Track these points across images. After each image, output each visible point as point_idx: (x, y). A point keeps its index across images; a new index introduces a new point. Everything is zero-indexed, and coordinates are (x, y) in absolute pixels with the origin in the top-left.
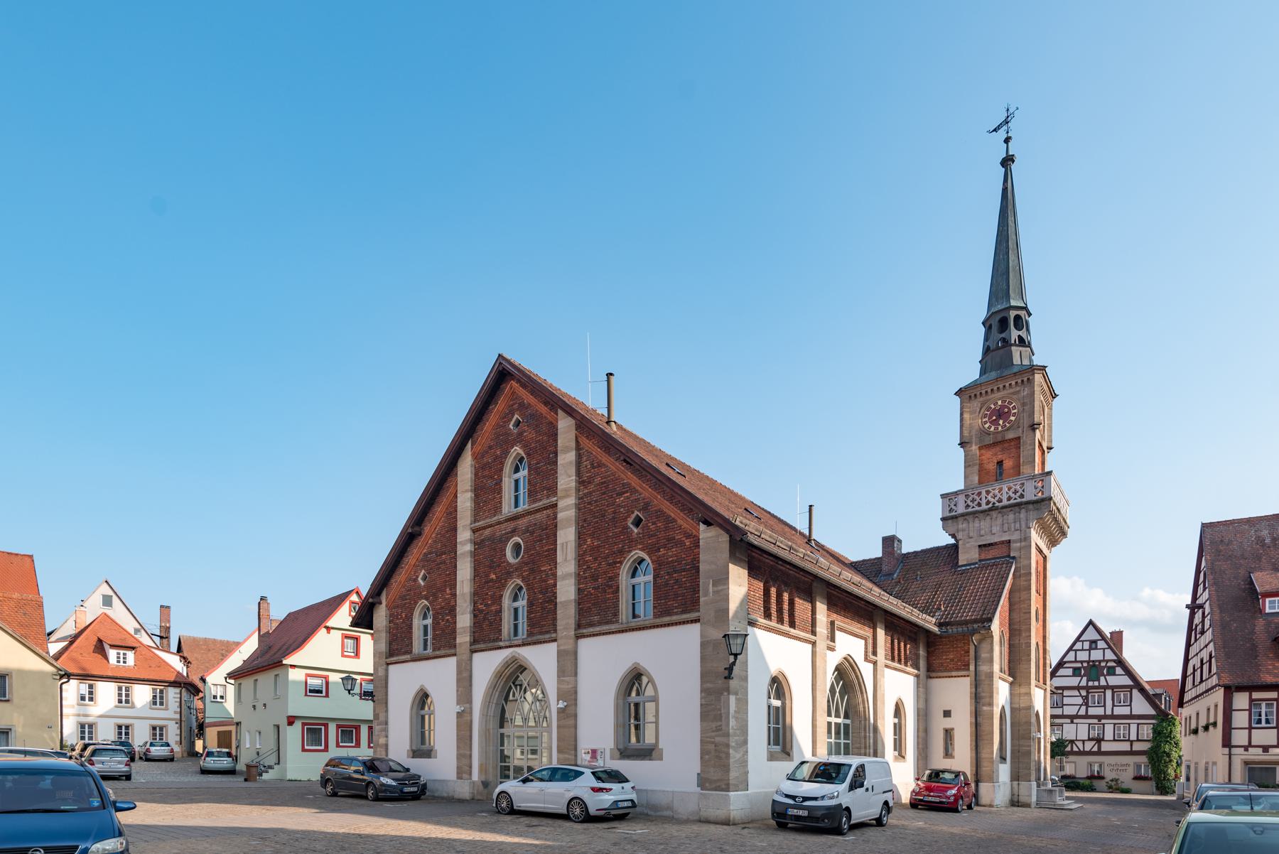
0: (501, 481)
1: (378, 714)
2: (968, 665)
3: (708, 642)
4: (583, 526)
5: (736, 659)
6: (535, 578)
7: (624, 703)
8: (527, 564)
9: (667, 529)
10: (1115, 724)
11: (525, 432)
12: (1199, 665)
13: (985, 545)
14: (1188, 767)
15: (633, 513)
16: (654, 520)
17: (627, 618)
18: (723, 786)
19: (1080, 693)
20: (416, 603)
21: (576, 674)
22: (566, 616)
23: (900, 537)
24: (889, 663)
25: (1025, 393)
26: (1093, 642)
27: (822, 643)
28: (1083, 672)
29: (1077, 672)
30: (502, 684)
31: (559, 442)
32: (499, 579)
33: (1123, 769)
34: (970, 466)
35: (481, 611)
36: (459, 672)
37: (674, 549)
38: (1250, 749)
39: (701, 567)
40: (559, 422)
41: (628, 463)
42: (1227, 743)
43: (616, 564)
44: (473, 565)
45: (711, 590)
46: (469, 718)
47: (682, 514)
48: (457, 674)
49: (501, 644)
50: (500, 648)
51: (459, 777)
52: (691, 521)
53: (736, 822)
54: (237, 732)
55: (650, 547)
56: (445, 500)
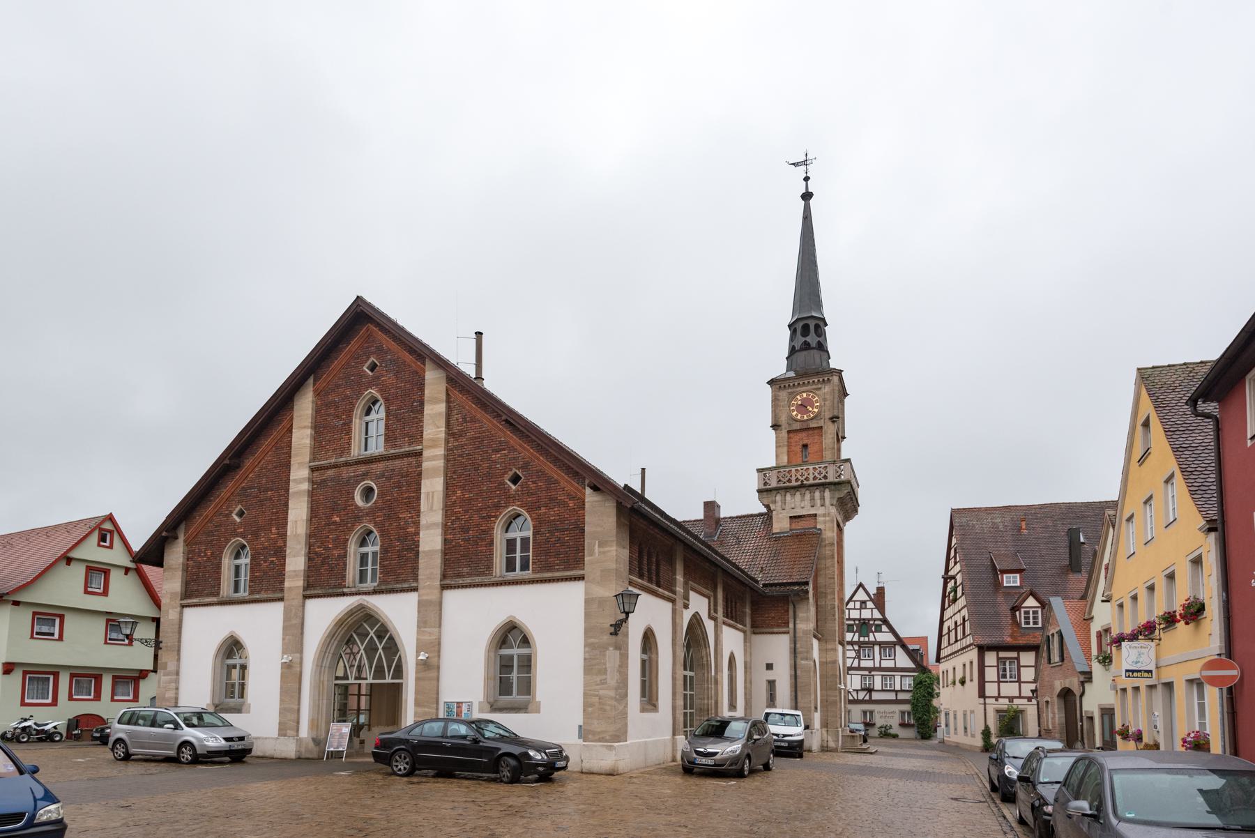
0: (351, 422)
2: (788, 623)
3: (593, 599)
7: (495, 656)
8: (381, 509)
9: (548, 489)
12: (953, 627)
13: (795, 517)
14: (947, 714)
17: (501, 571)
18: (608, 738)
20: (227, 541)
21: (440, 626)
25: (826, 390)
26: (863, 603)
27: (680, 603)
28: (855, 628)
29: (851, 628)
30: (342, 632)
32: (344, 523)
33: (889, 716)
34: (780, 446)
36: (287, 619)
37: (555, 509)
38: (1000, 699)
42: (982, 694)
43: (489, 518)
44: (310, 505)
48: (284, 621)
49: (345, 590)
50: (344, 594)
55: (530, 504)
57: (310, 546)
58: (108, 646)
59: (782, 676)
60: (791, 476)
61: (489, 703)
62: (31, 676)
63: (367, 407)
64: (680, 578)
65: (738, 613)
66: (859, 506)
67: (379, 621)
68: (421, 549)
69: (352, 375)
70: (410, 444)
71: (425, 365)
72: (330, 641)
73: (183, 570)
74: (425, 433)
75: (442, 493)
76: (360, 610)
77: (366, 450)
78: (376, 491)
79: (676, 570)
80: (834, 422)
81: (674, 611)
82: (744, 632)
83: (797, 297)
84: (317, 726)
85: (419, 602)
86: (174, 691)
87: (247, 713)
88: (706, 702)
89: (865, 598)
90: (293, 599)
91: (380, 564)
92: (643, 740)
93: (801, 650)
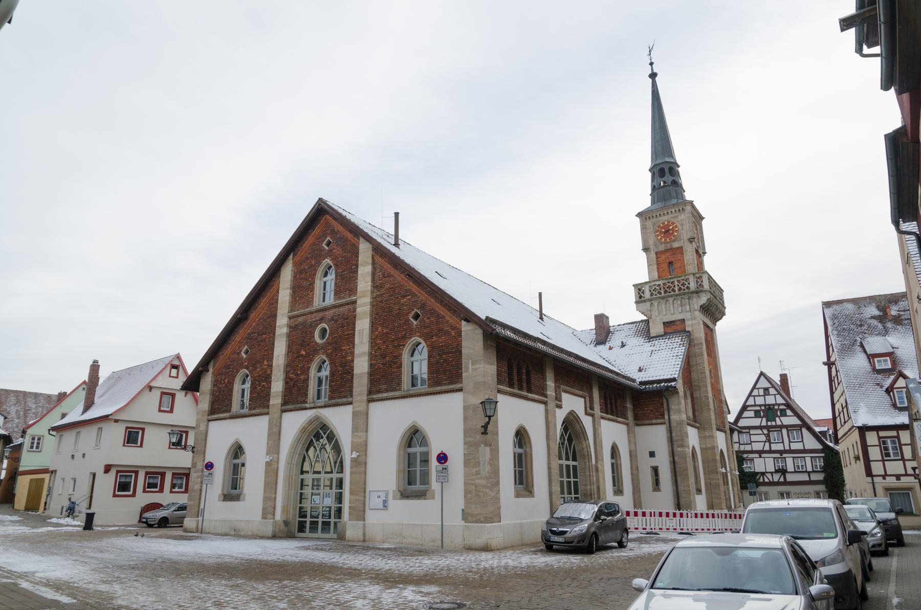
0: (314, 282)
1: (196, 463)
2: (664, 415)
4: (375, 318)
5: (490, 419)
6: (336, 355)
7: (404, 453)
9: (438, 323)
10: (794, 458)
11: (334, 249)
15: (413, 310)
16: (429, 316)
17: (408, 386)
19: (763, 432)
20: (238, 371)
21: (367, 431)
22: (361, 384)
23: (607, 314)
24: (604, 415)
25: (682, 218)
26: (766, 390)
27: (552, 404)
28: (762, 414)
29: (758, 414)
31: (360, 258)
34: (651, 265)
35: (292, 379)
37: (443, 337)
38: (886, 477)
39: (463, 351)
40: (360, 245)
41: (410, 276)
42: (869, 473)
43: (400, 347)
44: (287, 344)
45: (470, 368)
46: (276, 466)
47: (449, 313)
48: (269, 430)
49: (307, 405)
50: (306, 409)
51: (264, 517)
52: (456, 318)
53: (493, 548)
54: (50, 480)
56: (269, 294)
57: (287, 373)
58: (171, 450)
59: (663, 462)
60: (674, 286)
61: (400, 491)
62: (121, 474)
63: (324, 271)
64: (550, 384)
65: (619, 408)
66: (725, 308)
67: (329, 428)
68: (355, 372)
69: (317, 250)
70: (350, 296)
71: (359, 240)
72: (297, 444)
73: (210, 394)
74: (358, 287)
75: (368, 330)
76: (316, 420)
77: (324, 301)
78: (328, 329)
79: (546, 376)
80: (691, 242)
81: (547, 411)
82: (627, 424)
83: (654, 150)
84: (287, 511)
85: (353, 413)
86: (199, 485)
87: (243, 501)
88: (589, 487)
89: (768, 385)
90: (274, 413)
91: (329, 385)
92: (520, 521)
93: (676, 438)
